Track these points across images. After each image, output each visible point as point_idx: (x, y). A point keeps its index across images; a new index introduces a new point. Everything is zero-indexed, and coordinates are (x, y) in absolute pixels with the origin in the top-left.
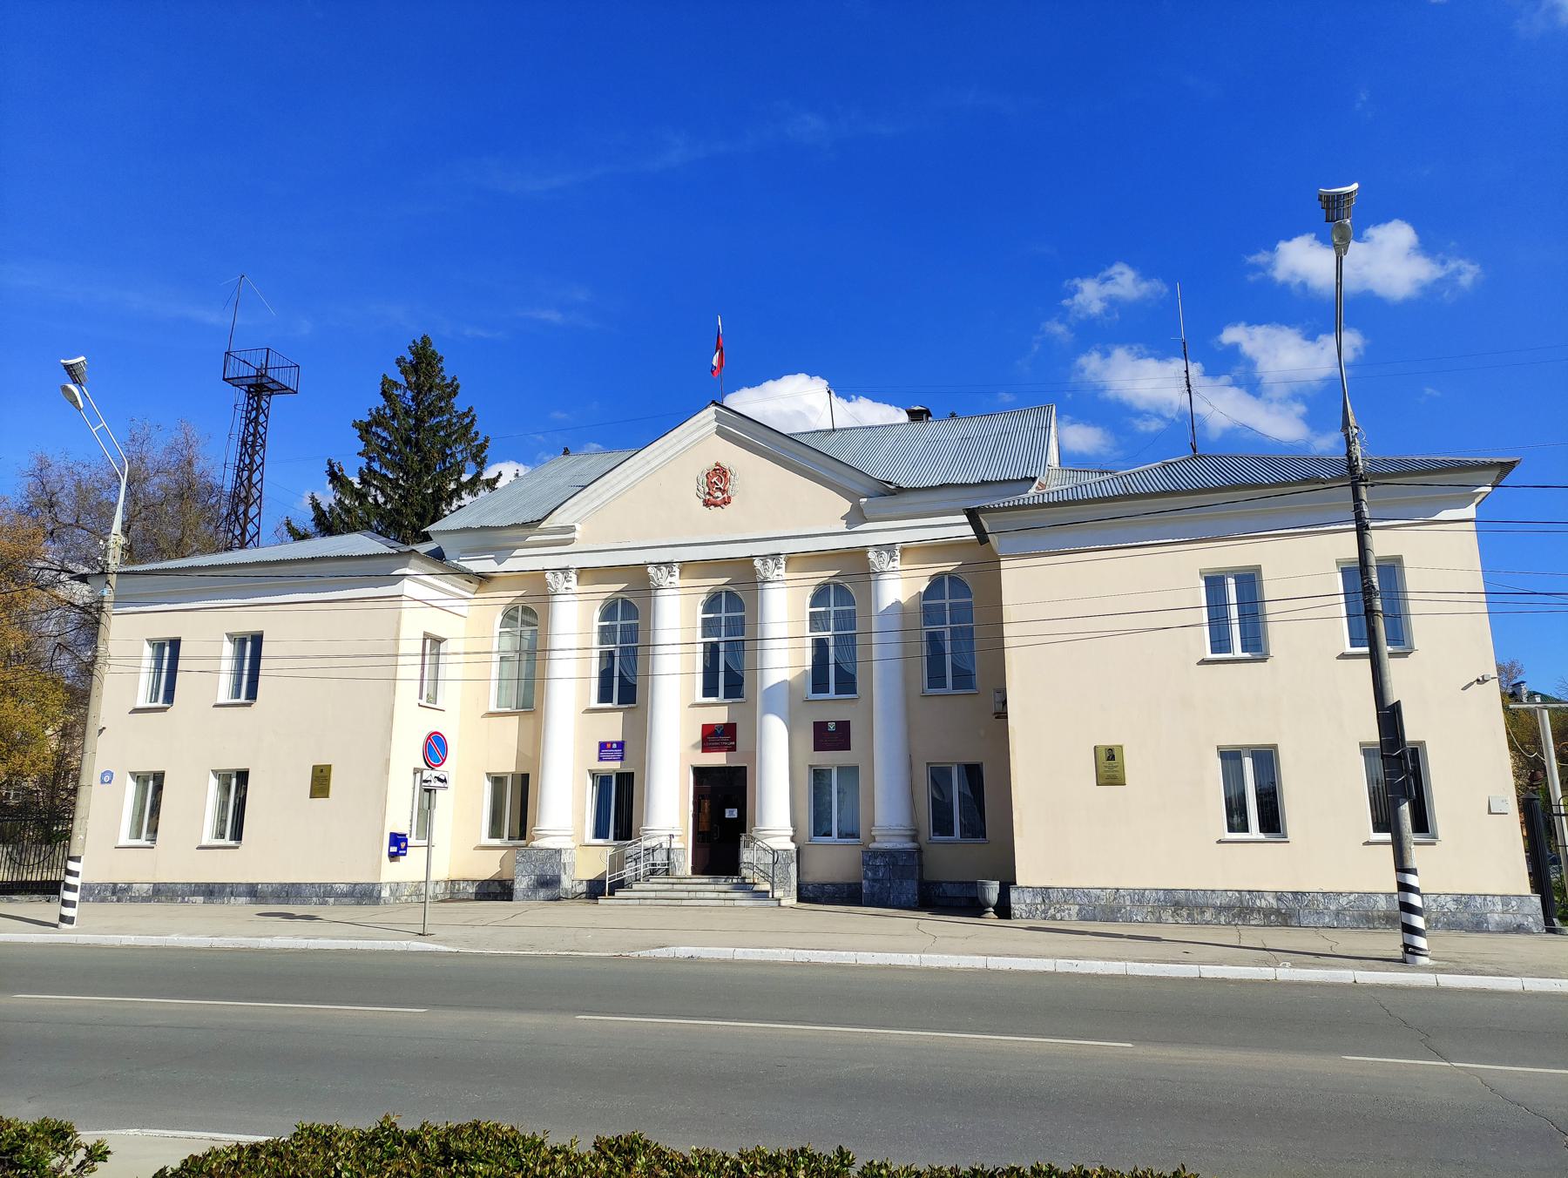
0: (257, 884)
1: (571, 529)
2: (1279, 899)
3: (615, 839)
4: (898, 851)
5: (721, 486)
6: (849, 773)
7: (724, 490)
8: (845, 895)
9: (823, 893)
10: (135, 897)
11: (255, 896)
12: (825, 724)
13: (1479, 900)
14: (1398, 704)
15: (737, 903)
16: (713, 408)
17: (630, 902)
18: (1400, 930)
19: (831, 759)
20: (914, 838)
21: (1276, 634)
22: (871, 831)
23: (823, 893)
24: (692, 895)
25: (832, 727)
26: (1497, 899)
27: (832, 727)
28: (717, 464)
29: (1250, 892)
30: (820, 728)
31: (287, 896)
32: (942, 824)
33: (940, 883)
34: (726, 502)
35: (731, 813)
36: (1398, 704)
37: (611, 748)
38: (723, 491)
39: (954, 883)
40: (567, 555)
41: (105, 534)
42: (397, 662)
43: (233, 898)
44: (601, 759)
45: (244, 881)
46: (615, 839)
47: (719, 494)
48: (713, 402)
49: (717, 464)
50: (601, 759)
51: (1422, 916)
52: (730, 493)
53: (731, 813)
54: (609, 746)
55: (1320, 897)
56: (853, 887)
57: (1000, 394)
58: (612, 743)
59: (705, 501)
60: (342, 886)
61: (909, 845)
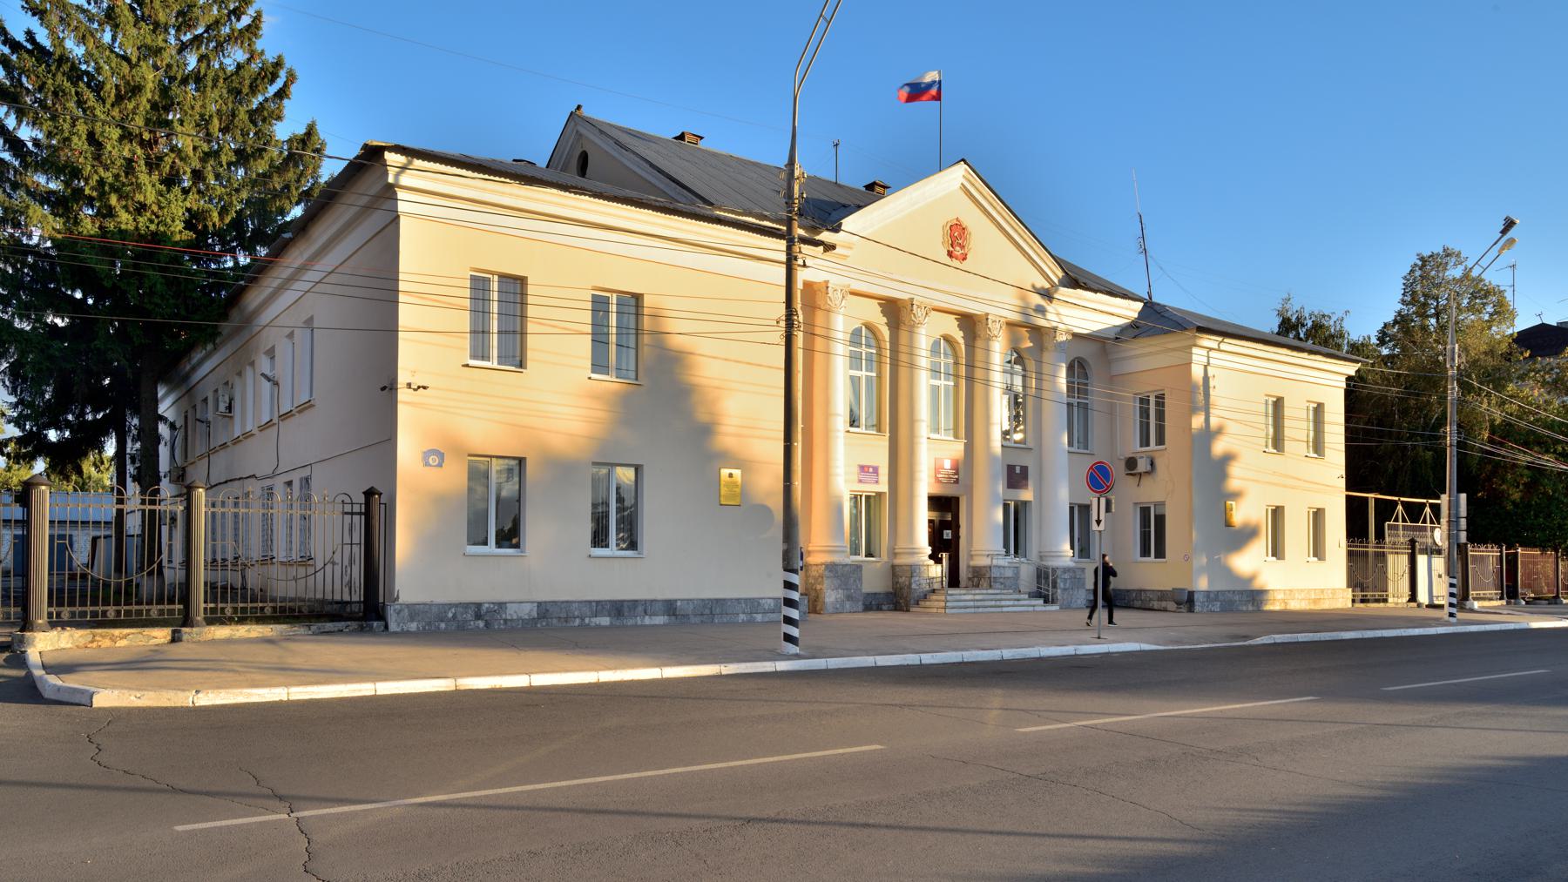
0: (676, 601)
3: (1156, 557)
5: (960, 242)
7: (964, 246)
10: (511, 620)
11: (674, 615)
16: (963, 166)
18: (28, 634)
21: (1287, 444)
22: (894, 549)
28: (957, 219)
31: (711, 613)
38: (962, 247)
41: (242, 42)
43: (647, 617)
45: (660, 597)
46: (1156, 557)
47: (958, 248)
48: (963, 160)
50: (860, 481)
51: (797, 609)
54: (866, 469)
58: (869, 467)
59: (948, 251)
60: (769, 601)
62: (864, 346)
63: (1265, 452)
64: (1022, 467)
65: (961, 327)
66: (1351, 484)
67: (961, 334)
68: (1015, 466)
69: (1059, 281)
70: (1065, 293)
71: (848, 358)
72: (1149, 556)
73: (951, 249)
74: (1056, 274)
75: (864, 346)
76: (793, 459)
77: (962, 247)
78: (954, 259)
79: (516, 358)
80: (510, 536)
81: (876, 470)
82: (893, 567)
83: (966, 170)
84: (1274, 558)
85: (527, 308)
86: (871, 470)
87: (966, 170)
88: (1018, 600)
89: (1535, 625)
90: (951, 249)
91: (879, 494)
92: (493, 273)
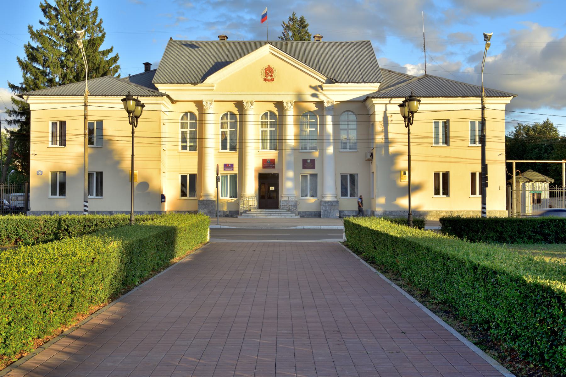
1: (213, 86)
2: (446, 213)
3: (96, 196)
4: (333, 201)
5: (270, 74)
6: (314, 176)
8: (313, 215)
9: (306, 214)
12: (307, 160)
13: (494, 212)
14: (487, 164)
15: (293, 217)
16: (268, 45)
17: (249, 217)
19: (308, 172)
20: (336, 197)
23: (306, 214)
24: (269, 215)
25: (309, 161)
26: (498, 212)
27: (309, 161)
28: (269, 66)
29: (439, 211)
30: (305, 161)
32: (344, 193)
33: (344, 211)
34: (272, 80)
35: (272, 188)
36: (487, 164)
37: (229, 166)
38: (271, 76)
39: (348, 211)
40: (455, 156)
42: (160, 135)
44: (225, 170)
47: (269, 77)
49: (269, 66)
50: (225, 170)
52: (274, 77)
53: (272, 188)
54: (227, 165)
55: (457, 212)
56: (316, 213)
57: (513, 137)
58: (229, 164)
61: (336, 200)
62: (189, 122)
63: (432, 146)
64: (311, 160)
65: (276, 107)
66: (507, 158)
67: (277, 109)
68: (307, 160)
69: (326, 81)
70: (326, 87)
71: (104, 134)
72: (56, 195)
73: (265, 78)
74: (323, 79)
75: (189, 122)
76: (245, 163)
77: (271, 76)
78: (267, 82)
79: (63, 143)
80: (63, 192)
81: (232, 165)
82: (321, 201)
83: (270, 46)
84: (445, 196)
85: (205, 115)
86: (230, 165)
87: (270, 46)
88: (281, 214)
89: (307, 227)
90: (265, 78)
91: (236, 175)
92: (58, 121)
